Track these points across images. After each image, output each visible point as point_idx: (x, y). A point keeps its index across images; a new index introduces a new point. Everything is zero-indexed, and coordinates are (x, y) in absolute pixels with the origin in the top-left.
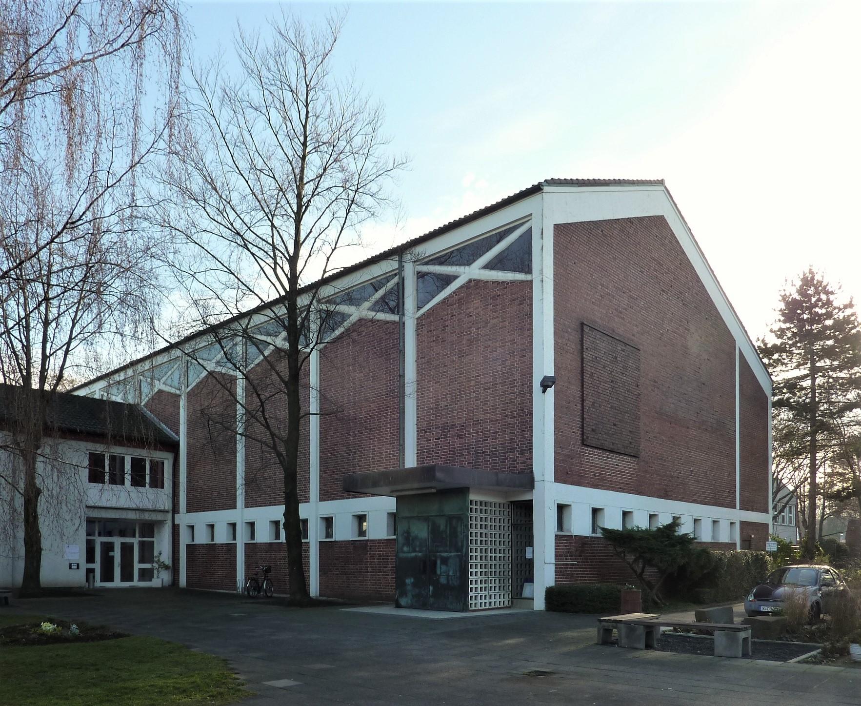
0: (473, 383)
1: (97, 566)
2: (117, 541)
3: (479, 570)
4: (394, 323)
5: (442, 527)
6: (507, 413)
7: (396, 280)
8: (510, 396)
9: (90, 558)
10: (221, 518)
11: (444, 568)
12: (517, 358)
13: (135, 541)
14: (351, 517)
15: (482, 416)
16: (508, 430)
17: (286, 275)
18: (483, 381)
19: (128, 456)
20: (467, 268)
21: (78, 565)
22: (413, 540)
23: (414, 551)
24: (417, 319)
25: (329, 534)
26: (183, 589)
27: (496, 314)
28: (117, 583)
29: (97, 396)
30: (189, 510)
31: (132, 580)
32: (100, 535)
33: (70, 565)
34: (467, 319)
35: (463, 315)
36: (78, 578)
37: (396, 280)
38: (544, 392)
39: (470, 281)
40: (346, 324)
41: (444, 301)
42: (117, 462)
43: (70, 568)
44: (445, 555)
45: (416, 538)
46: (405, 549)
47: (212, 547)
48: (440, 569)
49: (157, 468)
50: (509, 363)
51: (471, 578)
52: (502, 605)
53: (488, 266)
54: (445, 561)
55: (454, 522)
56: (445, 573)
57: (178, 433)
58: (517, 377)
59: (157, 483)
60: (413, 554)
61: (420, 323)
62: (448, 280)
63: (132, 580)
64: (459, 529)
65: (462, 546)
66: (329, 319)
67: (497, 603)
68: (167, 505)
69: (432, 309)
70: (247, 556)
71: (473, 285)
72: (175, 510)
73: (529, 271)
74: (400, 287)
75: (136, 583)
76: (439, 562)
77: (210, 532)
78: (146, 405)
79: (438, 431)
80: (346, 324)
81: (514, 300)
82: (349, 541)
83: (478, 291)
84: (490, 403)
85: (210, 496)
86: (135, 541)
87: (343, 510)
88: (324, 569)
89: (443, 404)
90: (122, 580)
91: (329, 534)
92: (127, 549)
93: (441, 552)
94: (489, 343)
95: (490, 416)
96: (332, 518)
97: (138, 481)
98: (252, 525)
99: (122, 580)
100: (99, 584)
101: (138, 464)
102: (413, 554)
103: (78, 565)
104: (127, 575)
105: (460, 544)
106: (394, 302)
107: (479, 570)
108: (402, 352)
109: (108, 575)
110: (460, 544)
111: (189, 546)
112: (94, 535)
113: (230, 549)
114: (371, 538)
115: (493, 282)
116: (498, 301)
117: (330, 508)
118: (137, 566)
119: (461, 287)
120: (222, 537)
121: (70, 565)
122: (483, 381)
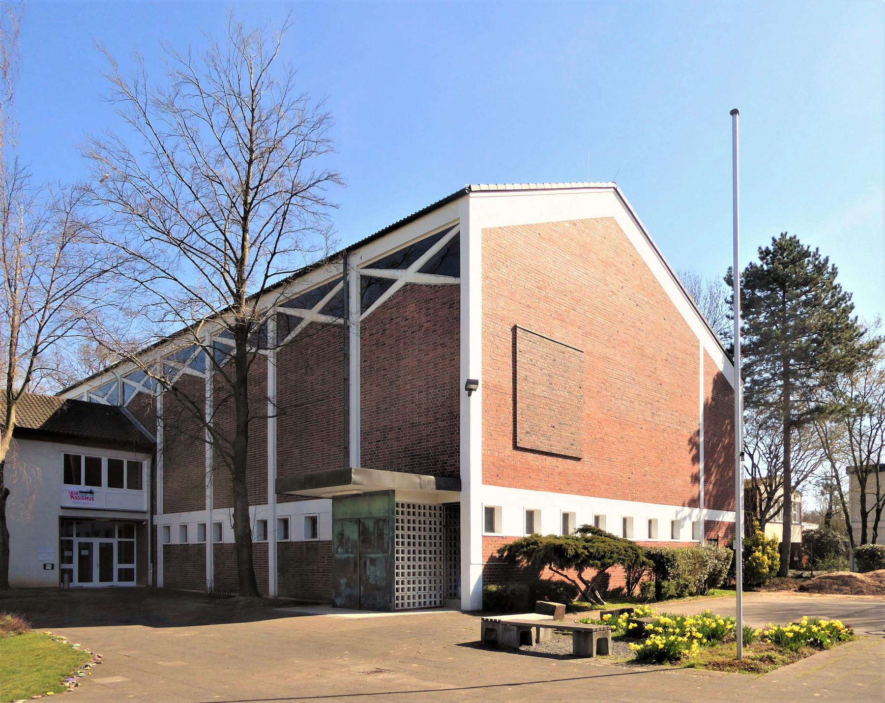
0: (408, 387)
1: (75, 566)
2: (96, 542)
3: (406, 571)
4: (339, 326)
5: (371, 529)
6: (438, 416)
7: (341, 285)
8: (441, 400)
9: (65, 559)
10: (192, 518)
11: (372, 568)
12: (447, 361)
13: (115, 541)
14: (303, 519)
15: (416, 419)
16: (439, 433)
17: (233, 279)
18: (417, 384)
19: (105, 456)
20: (404, 271)
21: (53, 565)
22: (346, 542)
23: (347, 552)
24: (362, 322)
25: (286, 536)
26: (160, 589)
27: (429, 318)
28: (96, 582)
29: (85, 399)
30: (165, 512)
31: (112, 580)
32: (78, 536)
33: (45, 565)
34: (403, 323)
35: (400, 319)
36: (53, 577)
37: (341, 285)
38: (469, 395)
39: (406, 285)
40: (298, 329)
41: (384, 305)
42: (94, 465)
43: (45, 568)
44: (372, 556)
45: (348, 539)
46: (340, 550)
47: (185, 548)
48: (370, 570)
49: (135, 468)
50: (440, 366)
51: (397, 578)
52: (433, 605)
53: (423, 270)
54: (373, 561)
55: (381, 524)
56: (375, 573)
57: (155, 436)
58: (447, 380)
59: (135, 484)
60: (346, 556)
61: (364, 326)
62: (387, 283)
63: (112, 580)
64: (385, 532)
65: (388, 547)
66: (286, 323)
67: (406, 605)
68: (145, 506)
69: (373, 313)
70: (216, 556)
71: (410, 288)
72: (153, 510)
73: (456, 274)
74: (345, 293)
75: (116, 582)
76: (368, 563)
77: (262, 529)
78: (128, 407)
79: (378, 433)
80: (298, 329)
81: (445, 303)
82: (302, 542)
83: (413, 294)
84: (424, 406)
85: (185, 499)
86: (115, 541)
87: (297, 512)
88: (282, 569)
89: (383, 407)
90: (101, 580)
91: (530, 527)
92: (106, 551)
93: (369, 553)
94: (423, 347)
95: (423, 419)
96: (486, 508)
97: (115, 481)
98: (285, 522)
99: (101, 580)
100: (76, 583)
101: (116, 466)
102: (346, 556)
103: (53, 565)
104: (106, 575)
105: (386, 546)
106: (339, 307)
107: (406, 571)
108: (347, 356)
109: (85, 576)
110: (386, 546)
111: (165, 547)
112: (119, 537)
113: (200, 549)
114: (226, 542)
115: (427, 286)
116: (431, 305)
117: (288, 509)
118: (117, 566)
119: (399, 291)
120: (193, 539)
121: (45, 565)
122: (417, 384)
